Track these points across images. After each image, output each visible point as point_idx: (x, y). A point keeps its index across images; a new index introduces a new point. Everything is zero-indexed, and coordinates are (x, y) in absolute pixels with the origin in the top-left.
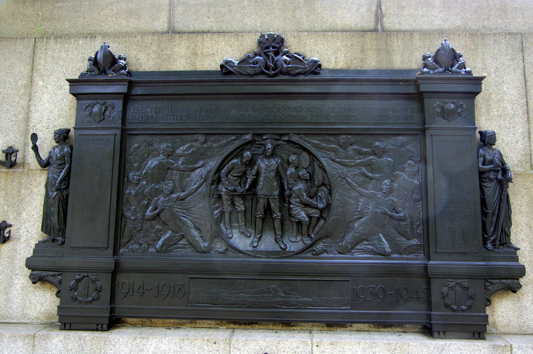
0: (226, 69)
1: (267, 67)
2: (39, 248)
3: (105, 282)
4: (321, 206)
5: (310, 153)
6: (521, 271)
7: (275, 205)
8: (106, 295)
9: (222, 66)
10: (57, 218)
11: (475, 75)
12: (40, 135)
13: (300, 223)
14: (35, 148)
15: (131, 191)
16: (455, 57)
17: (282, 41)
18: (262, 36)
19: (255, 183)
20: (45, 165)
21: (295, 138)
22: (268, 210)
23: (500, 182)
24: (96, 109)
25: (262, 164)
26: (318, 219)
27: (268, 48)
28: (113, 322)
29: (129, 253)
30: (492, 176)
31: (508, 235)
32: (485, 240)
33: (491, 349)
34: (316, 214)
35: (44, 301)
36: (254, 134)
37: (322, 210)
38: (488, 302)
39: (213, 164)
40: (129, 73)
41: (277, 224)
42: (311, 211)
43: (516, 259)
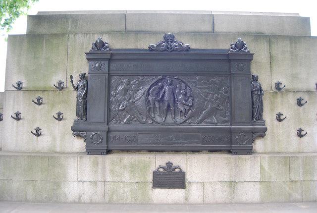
0: (151, 49)
1: (168, 48)
2: (76, 122)
3: (104, 135)
4: (190, 105)
5: (185, 83)
6: (266, 129)
7: (171, 105)
8: (105, 140)
9: (149, 47)
10: (83, 110)
11: (251, 52)
12: (73, 76)
13: (181, 112)
14: (72, 81)
15: (112, 99)
16: (243, 45)
17: (174, 37)
18: (166, 35)
19: (163, 96)
20: (77, 88)
21: (180, 78)
22: (169, 107)
23: (259, 95)
24: (97, 65)
25: (166, 88)
26: (189, 110)
27: (168, 40)
28: (109, 152)
29: (113, 125)
30: (256, 93)
31: (262, 116)
32: (253, 119)
33: (284, 167)
34: (187, 108)
35: (79, 144)
36: (163, 76)
37: (190, 107)
38: (253, 141)
39: (147, 88)
40: (110, 50)
41: (173, 112)
42: (186, 107)
43: (264, 125)
